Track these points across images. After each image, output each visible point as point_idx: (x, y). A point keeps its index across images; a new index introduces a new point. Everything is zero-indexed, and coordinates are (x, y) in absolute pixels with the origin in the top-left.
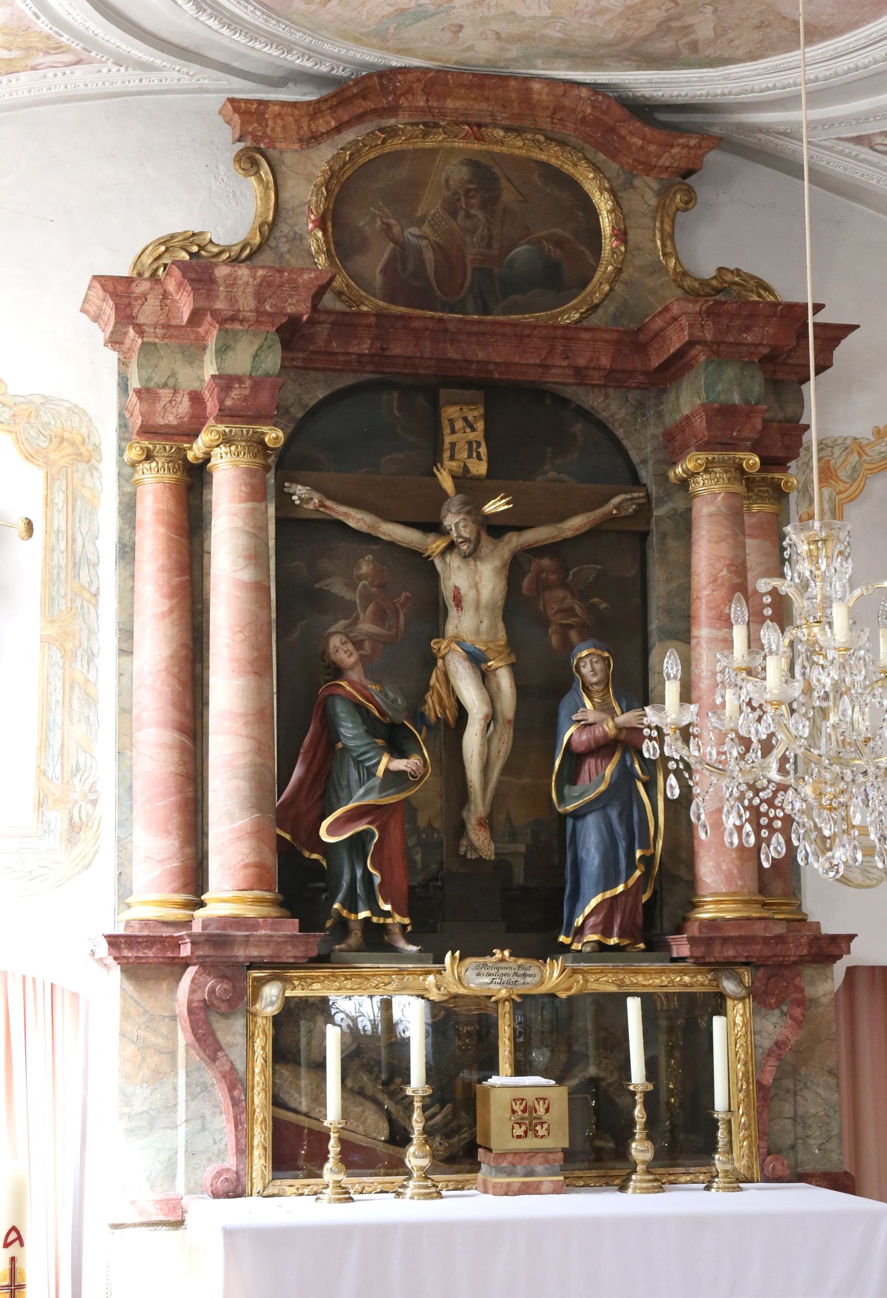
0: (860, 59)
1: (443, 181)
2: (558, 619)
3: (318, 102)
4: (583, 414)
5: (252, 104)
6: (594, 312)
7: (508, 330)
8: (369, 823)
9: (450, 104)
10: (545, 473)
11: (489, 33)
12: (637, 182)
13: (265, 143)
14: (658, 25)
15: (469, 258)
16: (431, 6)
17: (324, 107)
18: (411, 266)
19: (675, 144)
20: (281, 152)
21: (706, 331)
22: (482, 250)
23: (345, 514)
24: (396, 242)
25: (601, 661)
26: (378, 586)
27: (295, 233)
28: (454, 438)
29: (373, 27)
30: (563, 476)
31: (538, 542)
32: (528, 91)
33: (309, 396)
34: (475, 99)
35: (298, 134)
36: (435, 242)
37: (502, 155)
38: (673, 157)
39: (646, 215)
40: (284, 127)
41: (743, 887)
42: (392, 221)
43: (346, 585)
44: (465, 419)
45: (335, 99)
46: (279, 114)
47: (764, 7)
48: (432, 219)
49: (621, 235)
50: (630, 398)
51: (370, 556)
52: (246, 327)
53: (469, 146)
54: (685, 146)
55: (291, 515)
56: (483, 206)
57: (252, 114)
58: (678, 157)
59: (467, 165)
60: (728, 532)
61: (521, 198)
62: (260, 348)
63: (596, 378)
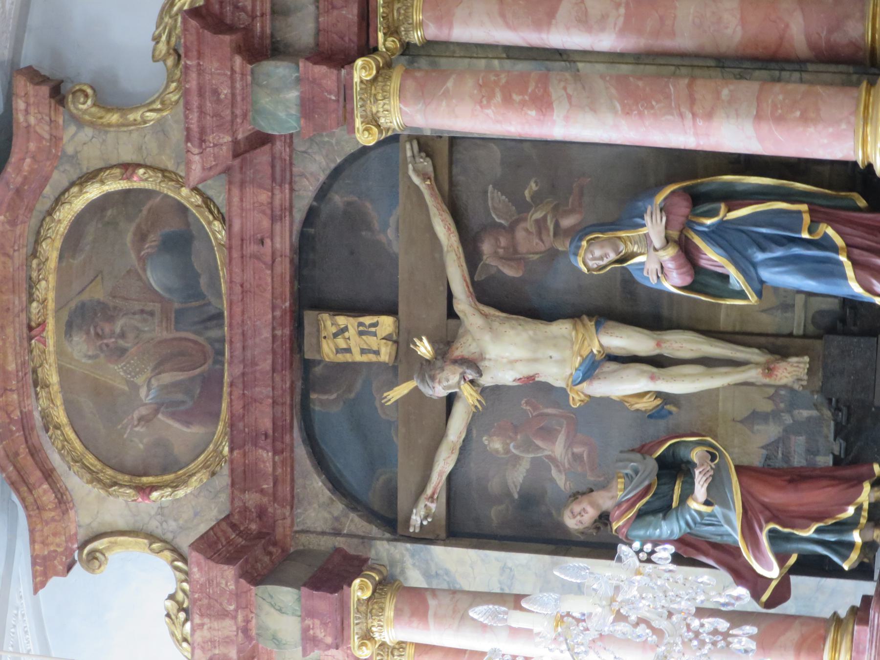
1: (90, 362)
2: (549, 238)
4: (323, 193)
5: (36, 571)
6: (211, 200)
7: (237, 310)
8: (761, 529)
9: (12, 367)
10: (390, 242)
12: (70, 150)
13: (73, 544)
15: (166, 335)
17: (30, 499)
18: (180, 397)
20: (80, 526)
21: (221, 141)
22: (156, 321)
23: (440, 475)
24: (157, 411)
25: (591, 248)
26: (516, 433)
27: (157, 514)
28: (356, 351)
30: (392, 221)
31: (463, 276)
33: (320, 496)
35: (60, 521)
36: (153, 370)
37: (57, 299)
38: (40, 121)
39: (104, 141)
40: (55, 534)
41: (849, 123)
42: (136, 415)
43: (514, 466)
44: (335, 335)
45: (21, 489)
46: (43, 543)
48: (129, 374)
49: (128, 168)
50: (302, 149)
51: (484, 438)
52: (253, 615)
54: (27, 112)
55: (443, 522)
56: (111, 319)
58: (39, 116)
59: (71, 336)
60: (444, 103)
61: (99, 278)
62: (273, 606)
63: (281, 197)
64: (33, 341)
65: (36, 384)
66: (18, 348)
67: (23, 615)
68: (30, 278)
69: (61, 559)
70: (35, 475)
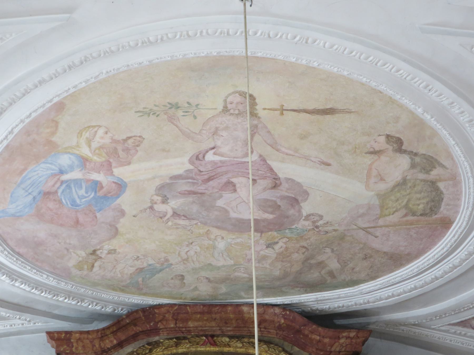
0: (437, 271)
3: (104, 329)
5: (62, 334)
9: (191, 324)
11: (202, 278)
14: (303, 263)
16: (158, 265)
17: (108, 332)
19: (341, 336)
29: (129, 281)
32: (241, 312)
34: (207, 320)
35: (93, 350)
38: (341, 345)
40: (83, 346)
45: (114, 327)
46: (79, 339)
47: (361, 246)
53: (208, 349)
54: (348, 337)
57: (62, 340)
58: (344, 345)
64: (204, 338)
65: (177, 338)
66: (200, 328)
67: (23, 324)
68: (243, 338)
69: (68, 350)
70: (122, 336)
